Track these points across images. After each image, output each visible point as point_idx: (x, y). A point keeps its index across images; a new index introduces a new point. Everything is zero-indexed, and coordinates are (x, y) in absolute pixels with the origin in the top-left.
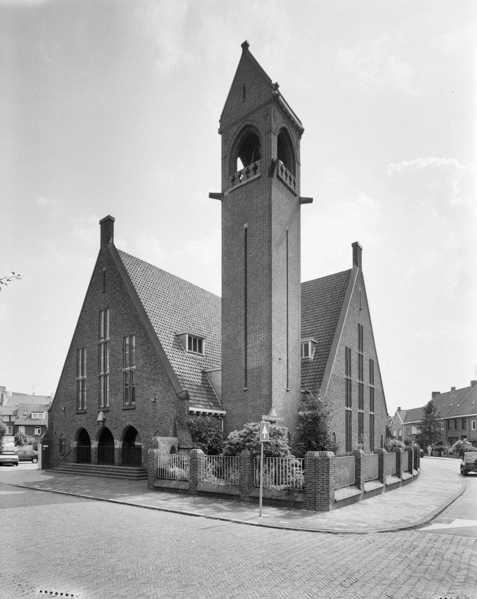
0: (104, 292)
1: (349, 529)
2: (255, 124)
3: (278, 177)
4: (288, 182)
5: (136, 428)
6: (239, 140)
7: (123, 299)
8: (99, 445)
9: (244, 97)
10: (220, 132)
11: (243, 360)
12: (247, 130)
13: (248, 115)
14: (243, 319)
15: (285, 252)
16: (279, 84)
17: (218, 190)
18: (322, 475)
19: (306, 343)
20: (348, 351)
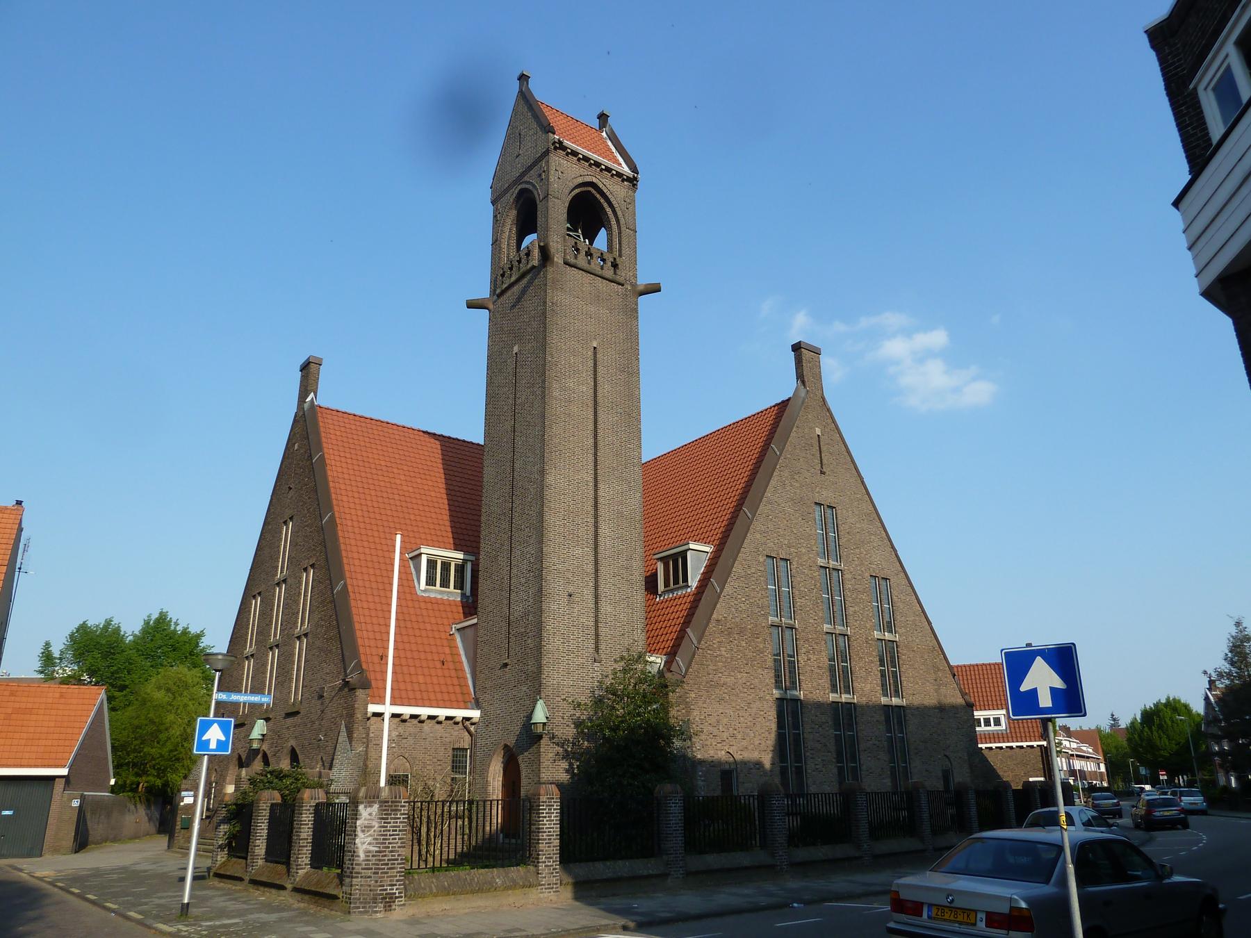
3: (566, 263)
5: (298, 752)
13: (523, 174)
15: (587, 389)
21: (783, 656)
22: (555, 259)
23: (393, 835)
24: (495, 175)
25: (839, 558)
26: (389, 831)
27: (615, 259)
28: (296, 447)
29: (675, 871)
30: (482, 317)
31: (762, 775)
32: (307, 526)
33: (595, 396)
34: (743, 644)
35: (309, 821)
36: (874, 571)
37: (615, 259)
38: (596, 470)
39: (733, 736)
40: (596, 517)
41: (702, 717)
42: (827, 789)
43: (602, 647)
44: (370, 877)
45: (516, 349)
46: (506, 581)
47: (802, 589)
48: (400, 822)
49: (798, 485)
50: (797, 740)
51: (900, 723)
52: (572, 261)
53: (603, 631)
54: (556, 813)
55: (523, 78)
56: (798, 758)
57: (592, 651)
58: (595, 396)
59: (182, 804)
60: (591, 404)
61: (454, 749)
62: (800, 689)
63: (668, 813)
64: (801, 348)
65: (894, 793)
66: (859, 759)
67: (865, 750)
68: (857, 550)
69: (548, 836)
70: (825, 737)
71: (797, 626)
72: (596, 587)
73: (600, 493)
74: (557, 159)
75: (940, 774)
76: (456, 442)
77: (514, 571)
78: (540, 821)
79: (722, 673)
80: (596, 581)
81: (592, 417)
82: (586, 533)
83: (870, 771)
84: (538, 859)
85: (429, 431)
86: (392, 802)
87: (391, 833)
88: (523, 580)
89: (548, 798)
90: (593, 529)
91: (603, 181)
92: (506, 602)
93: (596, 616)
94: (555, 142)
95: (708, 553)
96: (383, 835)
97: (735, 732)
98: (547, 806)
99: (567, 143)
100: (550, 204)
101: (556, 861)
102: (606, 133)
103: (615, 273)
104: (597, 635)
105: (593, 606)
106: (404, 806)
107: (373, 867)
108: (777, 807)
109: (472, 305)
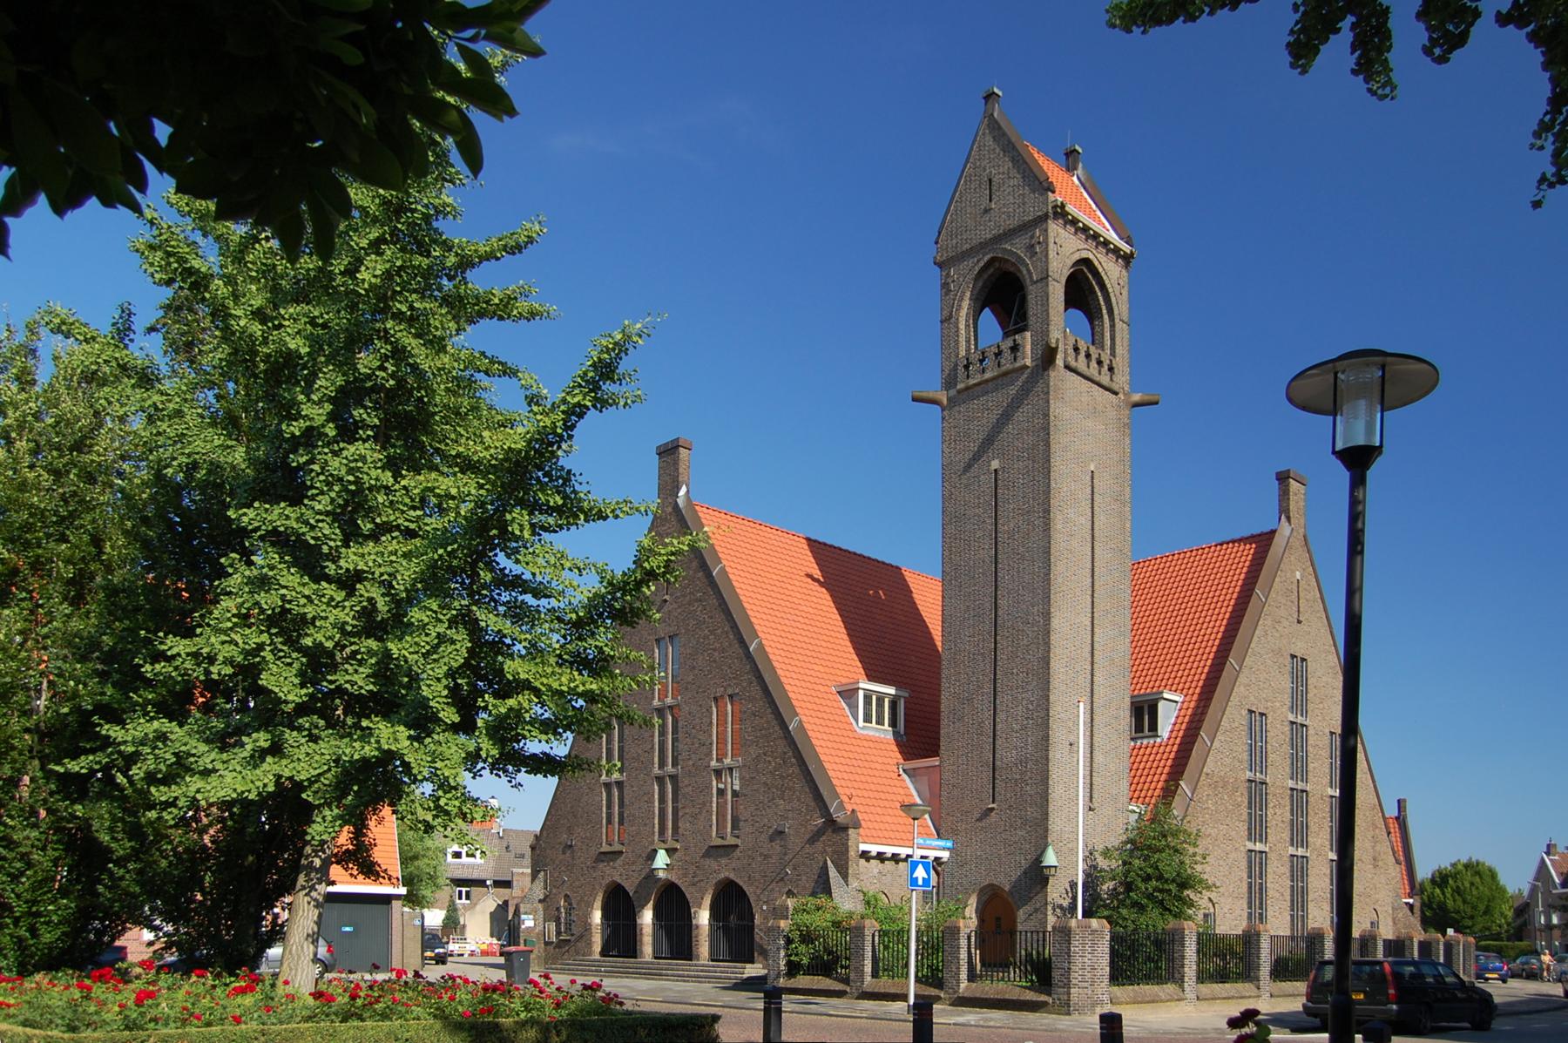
3: (1067, 367)
4: (1093, 370)
5: (741, 884)
11: (989, 747)
12: (997, 265)
15: (1085, 521)
16: (1128, 36)
19: (1151, 703)
20: (1257, 719)
24: (942, 227)
25: (1304, 713)
27: (1111, 361)
34: (1226, 797)
52: (1073, 364)
58: (1093, 529)
64: (1289, 477)
68: (1321, 706)
74: (1055, 228)
81: (1090, 554)
82: (1084, 680)
91: (1099, 256)
94: (1056, 206)
95: (1176, 702)
99: (1069, 208)
100: (1051, 288)
102: (1078, 178)
103: (1111, 380)
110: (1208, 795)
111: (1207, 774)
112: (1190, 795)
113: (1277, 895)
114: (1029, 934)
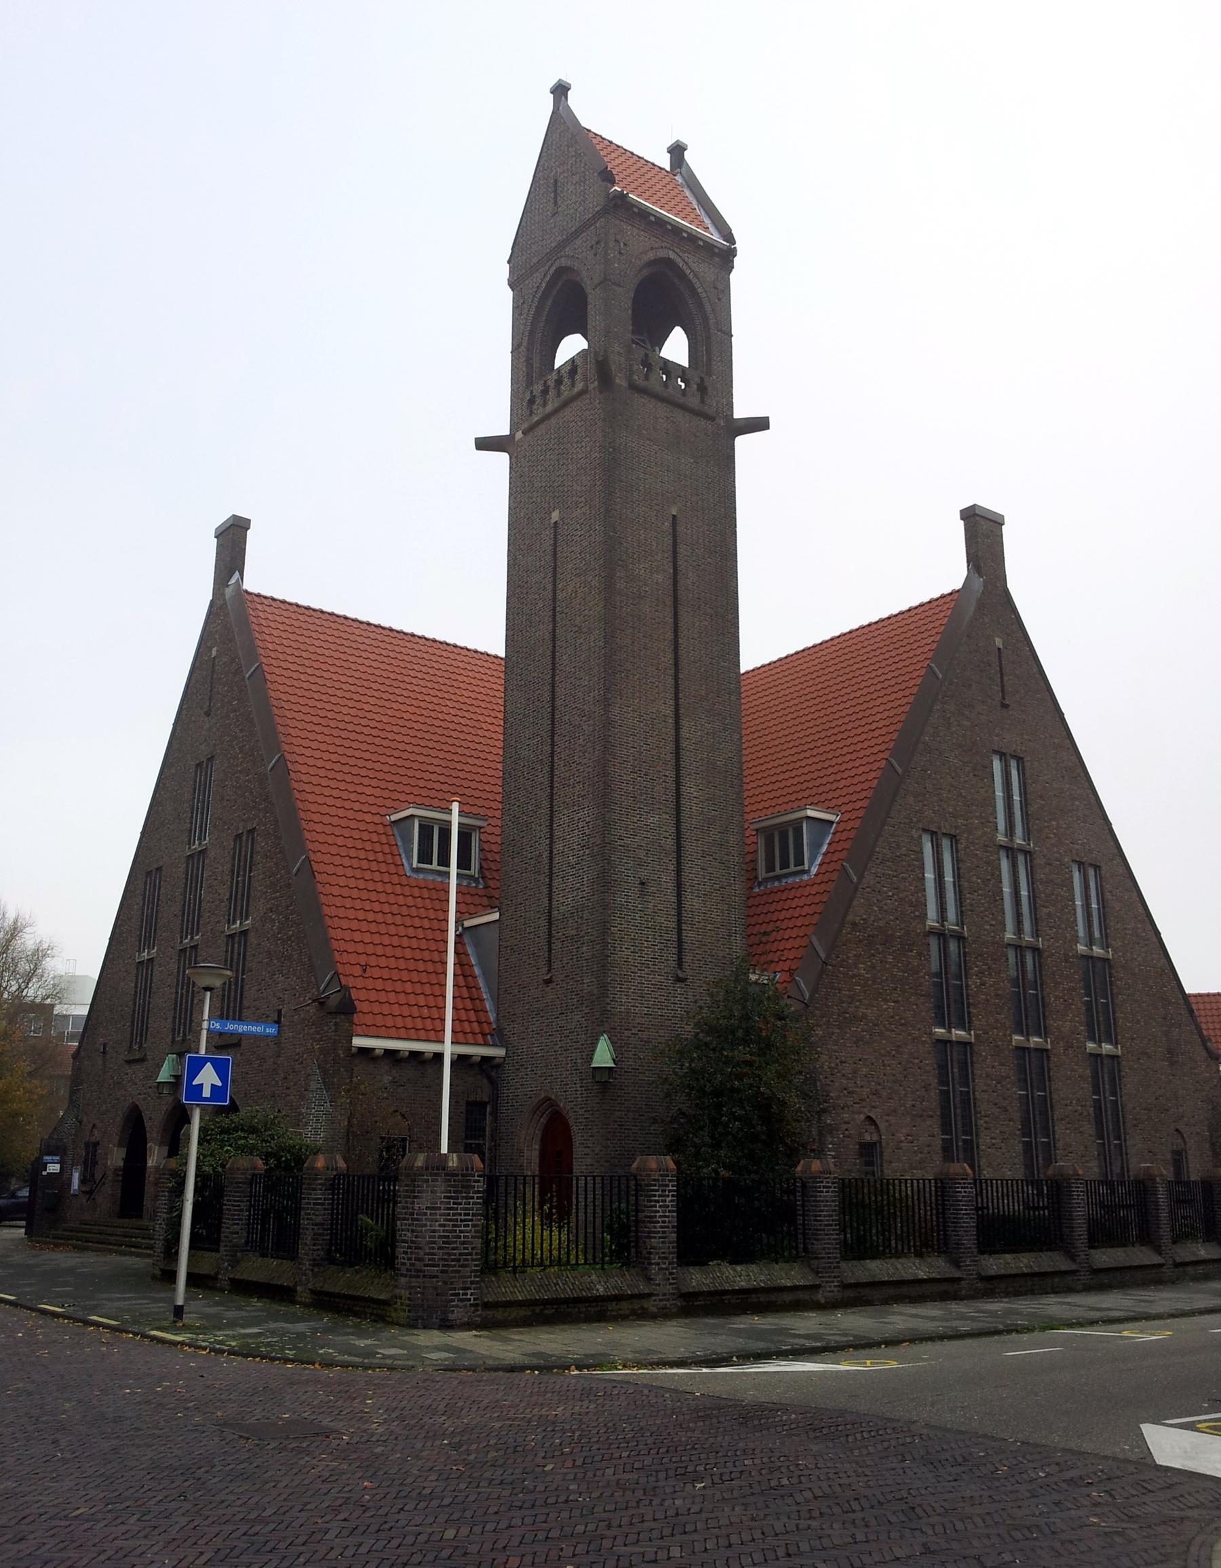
0: (208, 714)
1: (400, 1362)
2: (576, 265)
3: (633, 387)
6: (549, 303)
7: (241, 731)
8: (126, 1160)
9: (556, 203)
10: (512, 285)
13: (562, 245)
14: (547, 769)
17: (502, 428)
18: (432, 1220)
21: (946, 978)
22: (617, 381)
23: (465, 1220)
26: (460, 1214)
27: (702, 379)
28: (214, 653)
29: (827, 1282)
30: (502, 460)
31: (915, 1152)
32: (241, 772)
33: (675, 590)
35: (325, 1199)
36: (1077, 855)
37: (702, 379)
38: (677, 699)
39: (876, 1093)
40: (678, 768)
41: (833, 1065)
42: (1008, 1174)
43: (688, 958)
44: (435, 1277)
45: (555, 516)
46: (546, 861)
47: (974, 879)
48: (474, 1203)
49: (967, 723)
50: (967, 1101)
51: (1112, 1079)
53: (689, 935)
54: (673, 1196)
55: (561, 91)
56: (968, 1128)
57: (673, 964)
58: (675, 590)
59: (44, 1173)
60: (669, 601)
61: (468, 1103)
62: (970, 1026)
63: (817, 1201)
65: (1101, 1182)
66: (1054, 1132)
67: (1062, 1120)
69: (661, 1227)
70: (1005, 1099)
71: (966, 935)
72: (679, 871)
73: (684, 733)
75: (1169, 1156)
76: (443, 647)
77: (558, 846)
78: (651, 1207)
79: (860, 1001)
80: (679, 863)
81: (671, 621)
83: (1070, 1149)
84: (649, 1258)
85: (427, 636)
86: (462, 1175)
87: (463, 1218)
88: (573, 860)
89: (661, 1175)
90: (673, 787)
92: (545, 890)
93: (679, 914)
96: (450, 1220)
97: (879, 1087)
98: (660, 1186)
101: (673, 1263)
103: (703, 401)
104: (680, 941)
105: (674, 899)
106: (478, 1181)
107: (441, 1263)
108: (963, 1197)
109: (484, 444)
110: (858, 956)
111: (854, 924)
112: (823, 956)
113: (996, 1111)
114: (623, 1181)
